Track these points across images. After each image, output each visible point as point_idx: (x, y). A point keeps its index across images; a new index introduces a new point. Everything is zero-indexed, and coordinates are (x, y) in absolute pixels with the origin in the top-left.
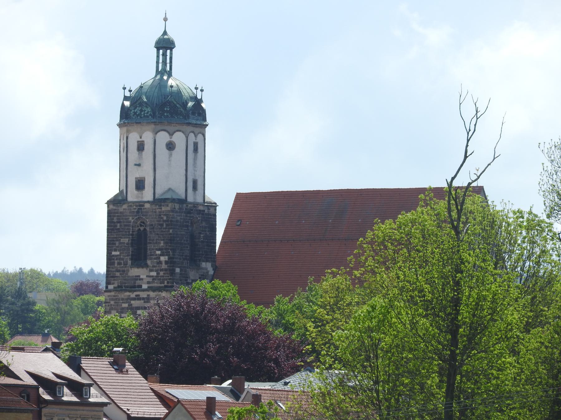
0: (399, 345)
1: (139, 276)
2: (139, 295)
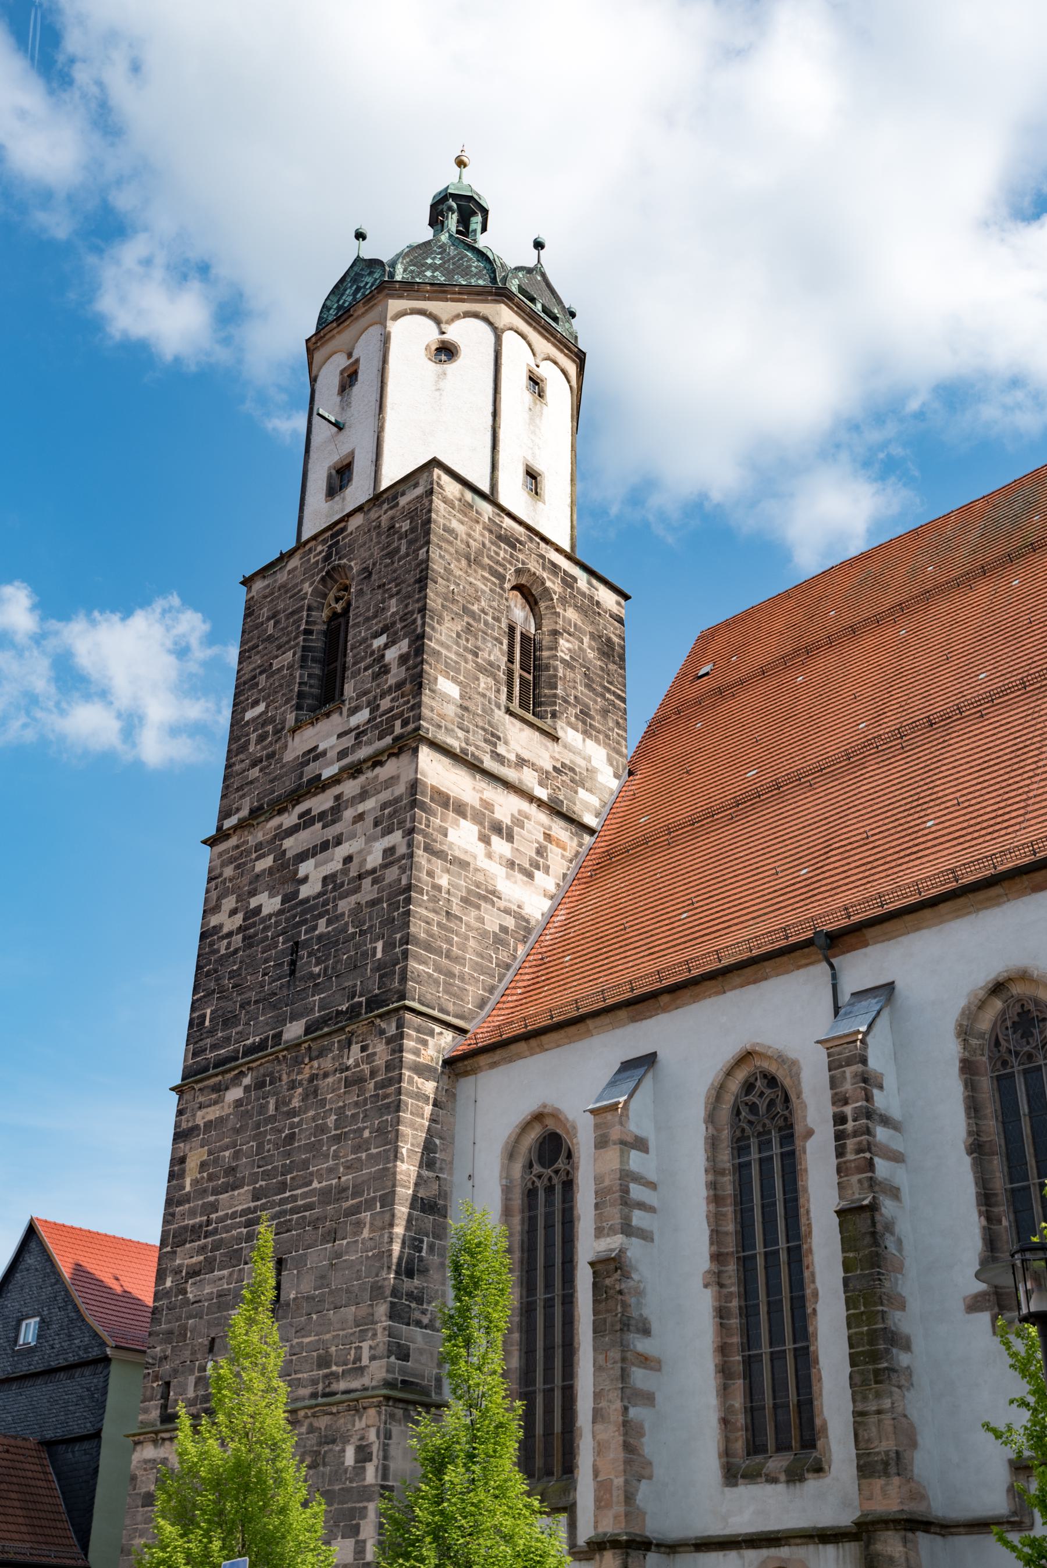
1: (317, 747)
2: (309, 811)
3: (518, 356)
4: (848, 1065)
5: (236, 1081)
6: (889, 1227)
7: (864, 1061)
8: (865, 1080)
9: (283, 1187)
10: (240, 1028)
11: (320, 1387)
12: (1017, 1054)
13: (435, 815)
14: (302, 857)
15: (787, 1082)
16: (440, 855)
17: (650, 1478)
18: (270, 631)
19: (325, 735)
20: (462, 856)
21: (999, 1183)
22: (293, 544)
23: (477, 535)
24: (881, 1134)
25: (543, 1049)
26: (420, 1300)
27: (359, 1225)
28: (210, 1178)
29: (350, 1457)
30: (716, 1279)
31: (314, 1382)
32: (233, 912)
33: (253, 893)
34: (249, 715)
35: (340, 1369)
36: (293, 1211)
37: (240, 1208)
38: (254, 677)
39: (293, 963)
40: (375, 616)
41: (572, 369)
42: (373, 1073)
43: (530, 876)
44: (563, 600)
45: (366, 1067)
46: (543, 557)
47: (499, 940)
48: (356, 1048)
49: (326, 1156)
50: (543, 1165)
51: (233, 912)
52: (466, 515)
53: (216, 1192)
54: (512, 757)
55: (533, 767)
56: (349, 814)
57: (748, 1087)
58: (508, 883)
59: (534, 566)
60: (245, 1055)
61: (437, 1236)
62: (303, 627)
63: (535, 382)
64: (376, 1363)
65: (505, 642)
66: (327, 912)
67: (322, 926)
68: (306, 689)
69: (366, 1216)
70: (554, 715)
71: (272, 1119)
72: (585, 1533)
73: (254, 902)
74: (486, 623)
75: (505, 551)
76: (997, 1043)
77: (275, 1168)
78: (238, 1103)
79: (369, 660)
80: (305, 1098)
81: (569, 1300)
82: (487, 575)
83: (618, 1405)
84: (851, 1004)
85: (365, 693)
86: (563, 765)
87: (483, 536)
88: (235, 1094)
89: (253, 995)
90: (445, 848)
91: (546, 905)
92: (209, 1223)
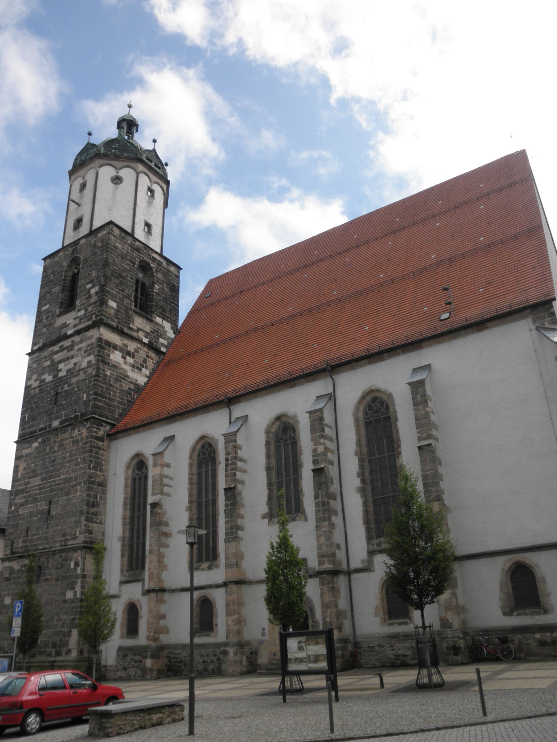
0: (88, 494)
1: (66, 323)
2: (62, 346)
3: (144, 181)
4: (230, 442)
5: (36, 440)
6: (240, 493)
7: (235, 441)
8: (235, 447)
9: (51, 477)
10: (37, 422)
11: (63, 543)
12: (282, 439)
13: (105, 350)
14: (60, 362)
15: (214, 446)
16: (108, 364)
17: (167, 570)
18: (52, 278)
19: (70, 319)
20: (116, 364)
21: (274, 479)
22: (60, 247)
23: (125, 248)
24: (239, 464)
25: (139, 432)
26: (96, 515)
27: (76, 490)
28: (27, 473)
29: (72, 565)
30: (190, 509)
31: (61, 541)
32: (36, 380)
33: (43, 374)
34: (43, 309)
35: (69, 538)
36: (55, 485)
37: (37, 484)
38: (45, 295)
39: (56, 400)
40: (88, 276)
41: (165, 187)
42: (82, 439)
43: (140, 370)
44: (157, 271)
45: (79, 438)
46: (150, 255)
47: (128, 392)
48: (76, 430)
49: (66, 467)
50: (138, 470)
51: (36, 380)
52: (121, 241)
53: (29, 478)
54: (135, 328)
55: (143, 331)
56: (76, 348)
57: (203, 447)
58: (132, 373)
59: (146, 259)
60: (39, 431)
61: (102, 494)
62: (63, 278)
63: (151, 190)
64: (81, 536)
65: (134, 286)
66: (68, 382)
67: (66, 387)
68: (63, 301)
69: (79, 487)
70: (152, 312)
71: (48, 454)
72: (146, 587)
73: (43, 377)
74: (128, 280)
75: (136, 254)
76: (277, 435)
77: (49, 471)
78: (37, 448)
79: (85, 293)
80: (59, 447)
81: (145, 515)
82: (128, 262)
83: (156, 548)
84: (234, 422)
85: (83, 304)
86: (154, 330)
87: (128, 248)
88: (36, 445)
89: (42, 410)
90: (109, 361)
91: (146, 380)
92: (26, 488)
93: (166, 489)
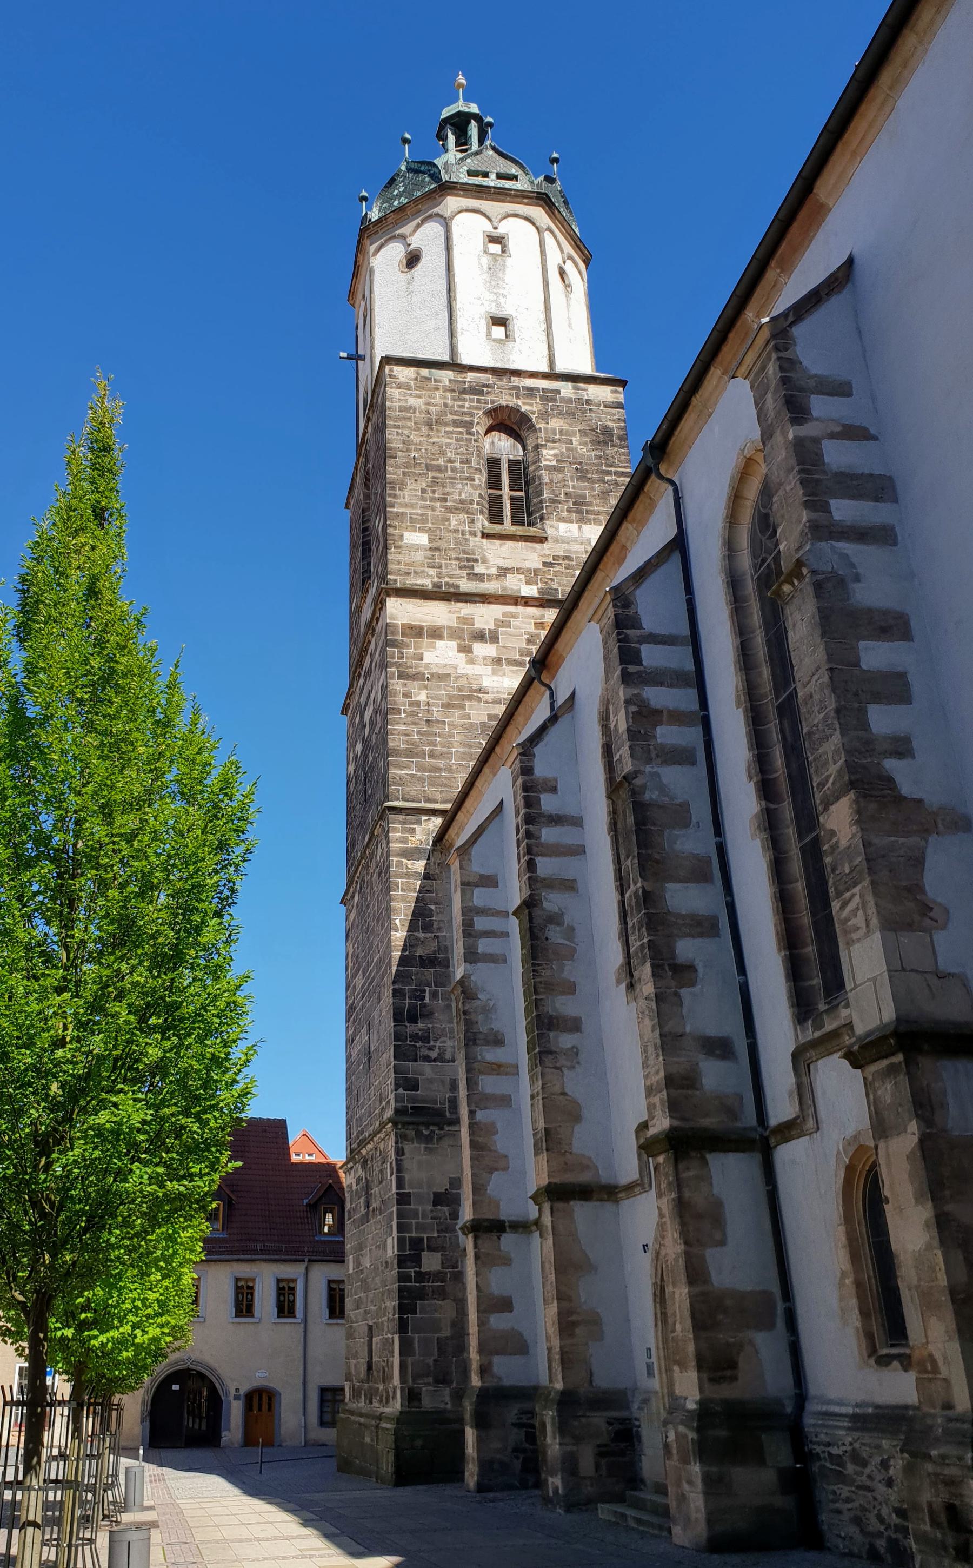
13: (408, 646)
20: (441, 671)
58: (495, 678)
82: (451, 429)
87: (444, 398)
90: (421, 670)
93: (483, 946)
